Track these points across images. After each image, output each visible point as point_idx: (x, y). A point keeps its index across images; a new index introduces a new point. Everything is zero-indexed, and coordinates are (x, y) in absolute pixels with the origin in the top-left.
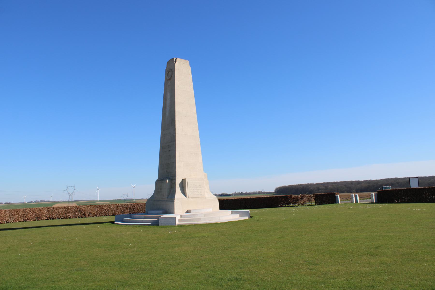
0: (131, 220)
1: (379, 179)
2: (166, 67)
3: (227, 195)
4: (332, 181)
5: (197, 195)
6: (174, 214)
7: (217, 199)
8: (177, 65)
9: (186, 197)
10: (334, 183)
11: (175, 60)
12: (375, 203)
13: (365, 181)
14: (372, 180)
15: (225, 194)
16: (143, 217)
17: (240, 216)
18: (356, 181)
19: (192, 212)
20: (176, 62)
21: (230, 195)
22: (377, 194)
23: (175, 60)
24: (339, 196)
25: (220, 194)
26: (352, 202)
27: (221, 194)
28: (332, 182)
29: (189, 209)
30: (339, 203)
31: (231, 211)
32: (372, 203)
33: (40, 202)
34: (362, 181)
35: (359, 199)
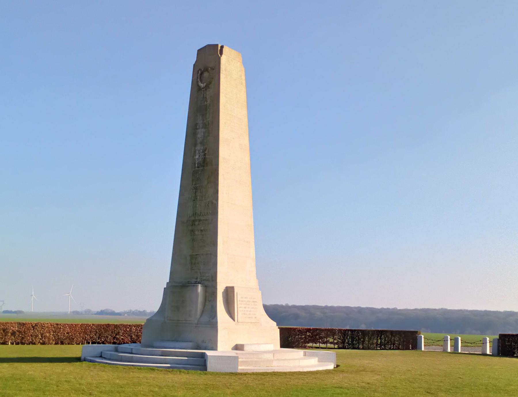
0: (129, 356)
1: (412, 308)
2: (195, 60)
3: (113, 313)
4: (323, 305)
5: (250, 318)
6: (243, 350)
7: (277, 327)
8: (224, 59)
9: (234, 320)
10: (326, 307)
11: (219, 48)
12: (492, 355)
13: (382, 310)
14: (398, 308)
15: (110, 311)
16: (160, 353)
17: (319, 361)
18: (368, 308)
19: (246, 348)
20: (221, 53)
21: (119, 314)
22: (498, 340)
23: (219, 48)
24: (423, 336)
25: (99, 310)
26: (445, 351)
27: (101, 311)
28: (323, 305)
29: (240, 342)
30: (423, 349)
31: (304, 352)
32: (485, 355)
33: (96, 314)
34: (284, 305)
35: (425, 346)
